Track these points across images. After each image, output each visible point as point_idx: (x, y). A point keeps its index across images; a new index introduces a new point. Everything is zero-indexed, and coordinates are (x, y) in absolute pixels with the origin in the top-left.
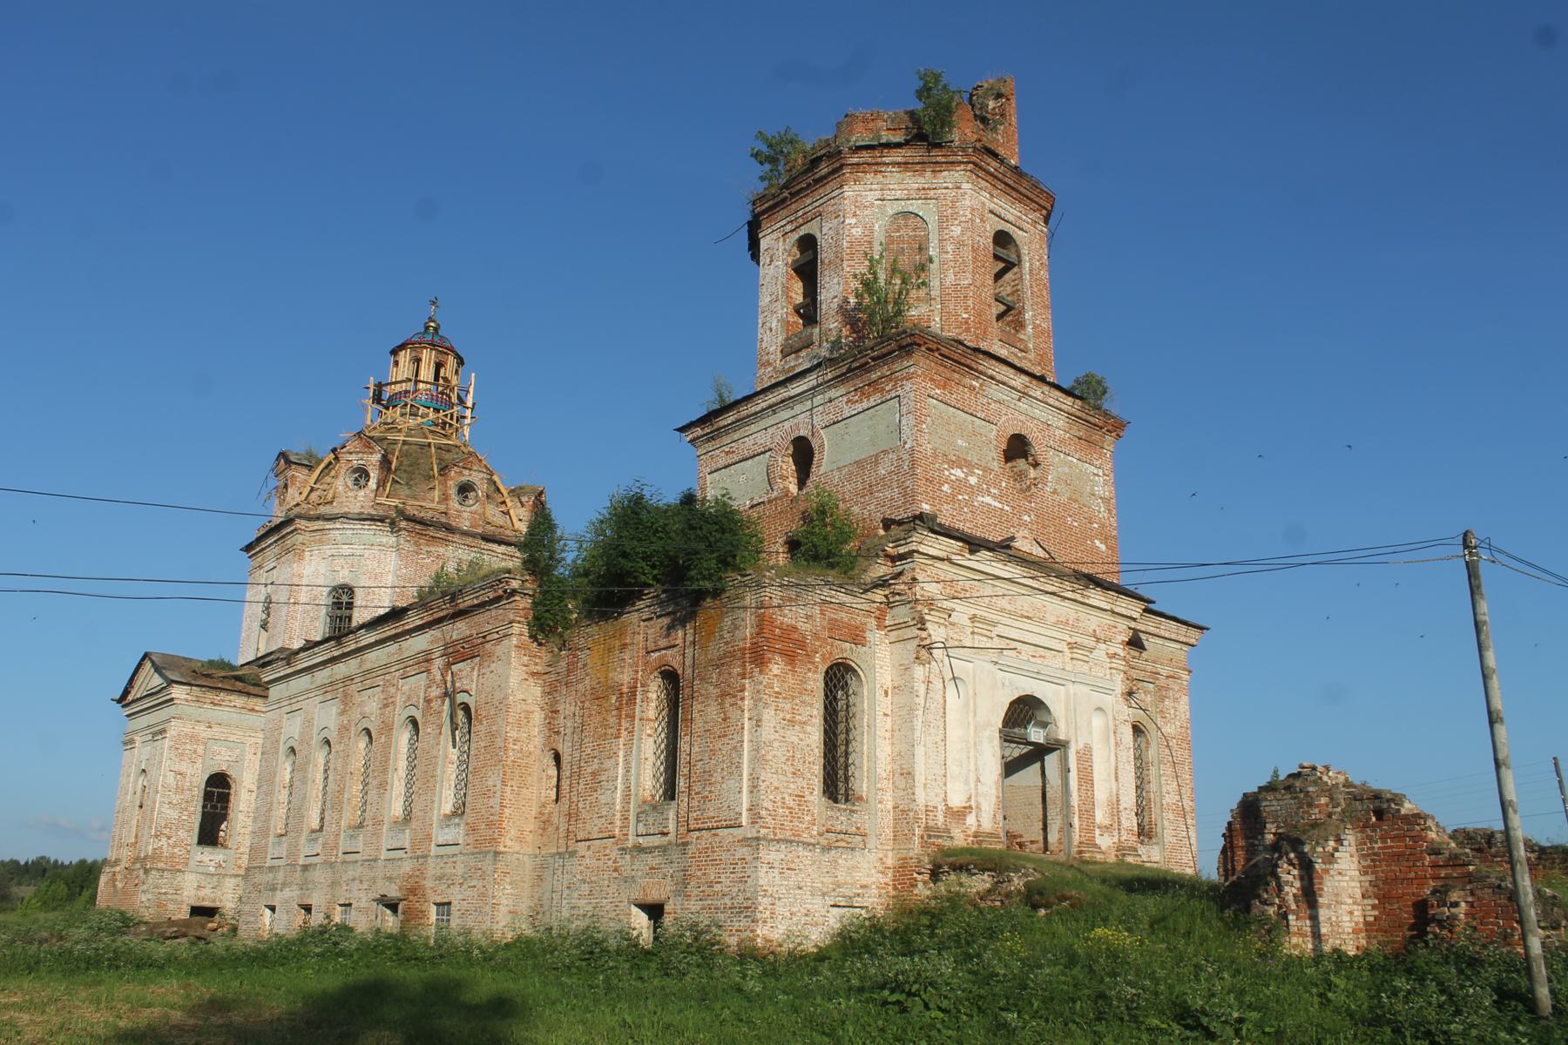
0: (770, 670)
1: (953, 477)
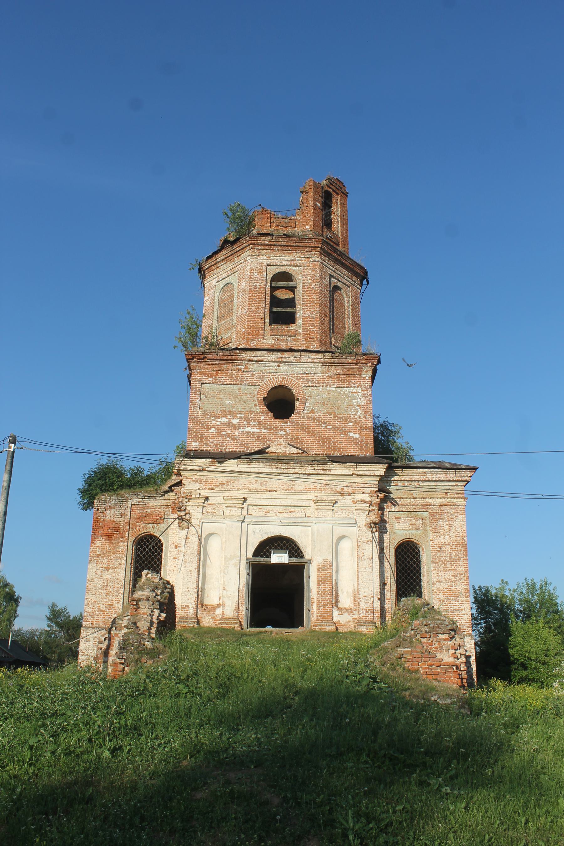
0: (95, 544)
1: (218, 423)
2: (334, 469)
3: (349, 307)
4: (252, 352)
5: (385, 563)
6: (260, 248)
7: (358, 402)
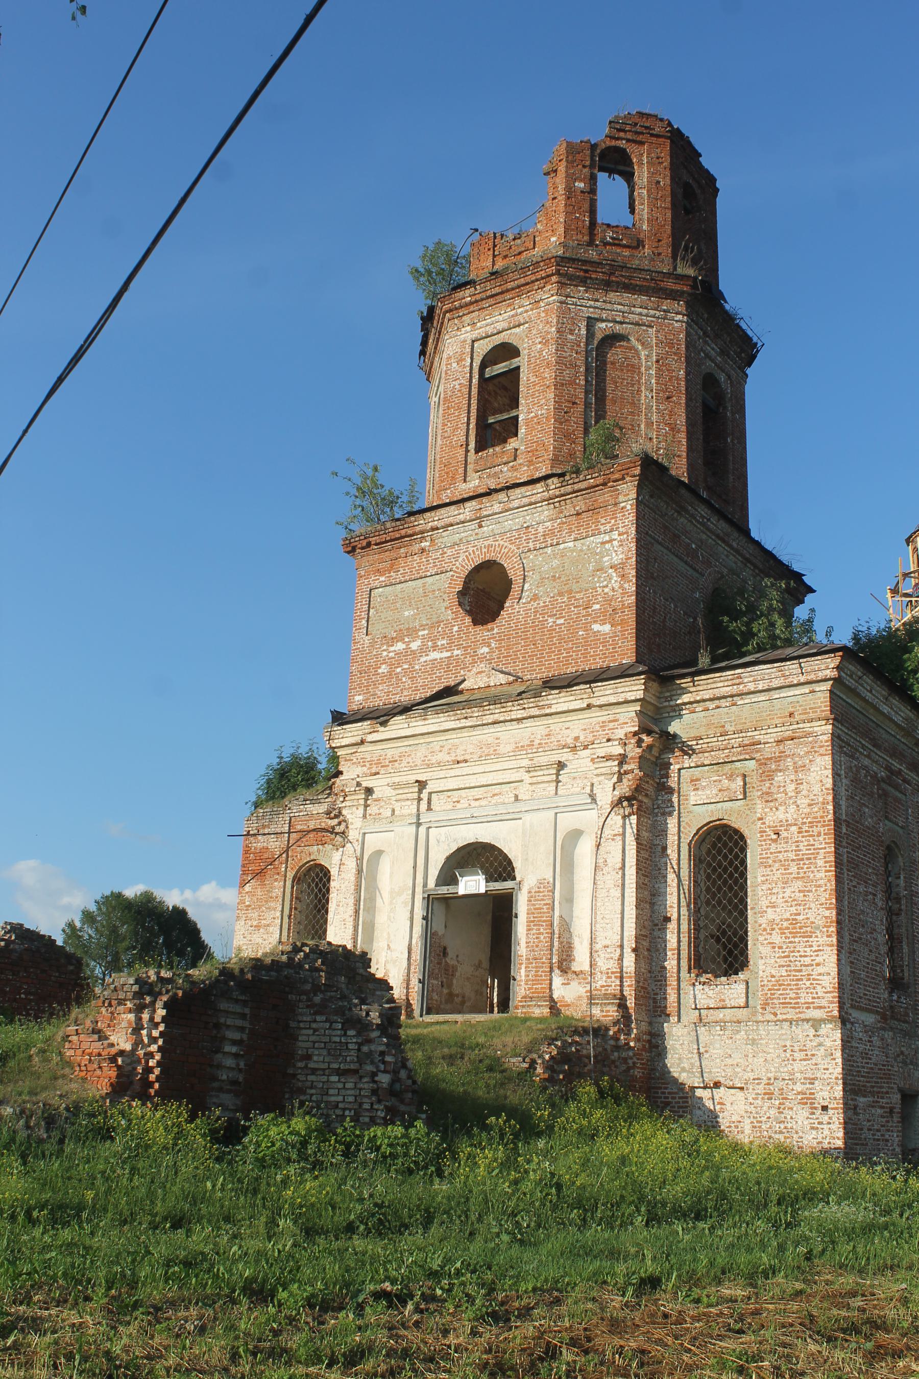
1: (392, 655)
2: (555, 701)
3: (648, 368)
4: (433, 514)
5: (669, 876)
6: (461, 314)
7: (611, 559)
